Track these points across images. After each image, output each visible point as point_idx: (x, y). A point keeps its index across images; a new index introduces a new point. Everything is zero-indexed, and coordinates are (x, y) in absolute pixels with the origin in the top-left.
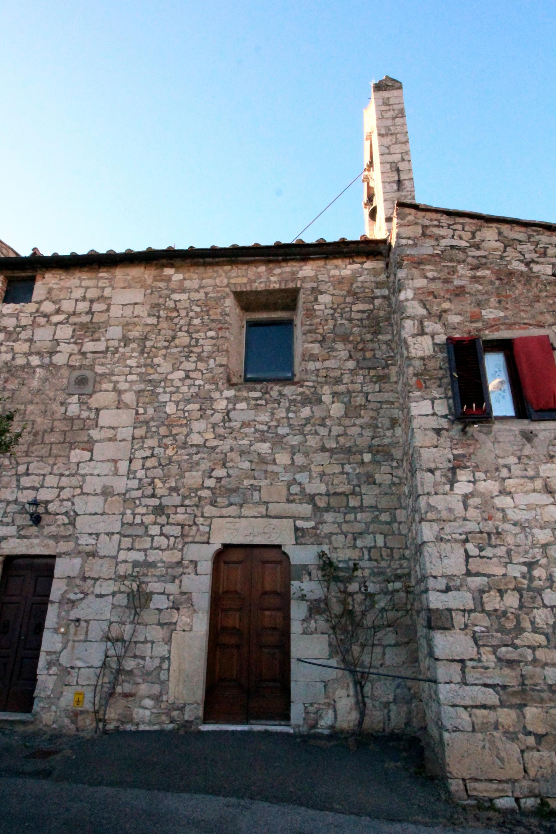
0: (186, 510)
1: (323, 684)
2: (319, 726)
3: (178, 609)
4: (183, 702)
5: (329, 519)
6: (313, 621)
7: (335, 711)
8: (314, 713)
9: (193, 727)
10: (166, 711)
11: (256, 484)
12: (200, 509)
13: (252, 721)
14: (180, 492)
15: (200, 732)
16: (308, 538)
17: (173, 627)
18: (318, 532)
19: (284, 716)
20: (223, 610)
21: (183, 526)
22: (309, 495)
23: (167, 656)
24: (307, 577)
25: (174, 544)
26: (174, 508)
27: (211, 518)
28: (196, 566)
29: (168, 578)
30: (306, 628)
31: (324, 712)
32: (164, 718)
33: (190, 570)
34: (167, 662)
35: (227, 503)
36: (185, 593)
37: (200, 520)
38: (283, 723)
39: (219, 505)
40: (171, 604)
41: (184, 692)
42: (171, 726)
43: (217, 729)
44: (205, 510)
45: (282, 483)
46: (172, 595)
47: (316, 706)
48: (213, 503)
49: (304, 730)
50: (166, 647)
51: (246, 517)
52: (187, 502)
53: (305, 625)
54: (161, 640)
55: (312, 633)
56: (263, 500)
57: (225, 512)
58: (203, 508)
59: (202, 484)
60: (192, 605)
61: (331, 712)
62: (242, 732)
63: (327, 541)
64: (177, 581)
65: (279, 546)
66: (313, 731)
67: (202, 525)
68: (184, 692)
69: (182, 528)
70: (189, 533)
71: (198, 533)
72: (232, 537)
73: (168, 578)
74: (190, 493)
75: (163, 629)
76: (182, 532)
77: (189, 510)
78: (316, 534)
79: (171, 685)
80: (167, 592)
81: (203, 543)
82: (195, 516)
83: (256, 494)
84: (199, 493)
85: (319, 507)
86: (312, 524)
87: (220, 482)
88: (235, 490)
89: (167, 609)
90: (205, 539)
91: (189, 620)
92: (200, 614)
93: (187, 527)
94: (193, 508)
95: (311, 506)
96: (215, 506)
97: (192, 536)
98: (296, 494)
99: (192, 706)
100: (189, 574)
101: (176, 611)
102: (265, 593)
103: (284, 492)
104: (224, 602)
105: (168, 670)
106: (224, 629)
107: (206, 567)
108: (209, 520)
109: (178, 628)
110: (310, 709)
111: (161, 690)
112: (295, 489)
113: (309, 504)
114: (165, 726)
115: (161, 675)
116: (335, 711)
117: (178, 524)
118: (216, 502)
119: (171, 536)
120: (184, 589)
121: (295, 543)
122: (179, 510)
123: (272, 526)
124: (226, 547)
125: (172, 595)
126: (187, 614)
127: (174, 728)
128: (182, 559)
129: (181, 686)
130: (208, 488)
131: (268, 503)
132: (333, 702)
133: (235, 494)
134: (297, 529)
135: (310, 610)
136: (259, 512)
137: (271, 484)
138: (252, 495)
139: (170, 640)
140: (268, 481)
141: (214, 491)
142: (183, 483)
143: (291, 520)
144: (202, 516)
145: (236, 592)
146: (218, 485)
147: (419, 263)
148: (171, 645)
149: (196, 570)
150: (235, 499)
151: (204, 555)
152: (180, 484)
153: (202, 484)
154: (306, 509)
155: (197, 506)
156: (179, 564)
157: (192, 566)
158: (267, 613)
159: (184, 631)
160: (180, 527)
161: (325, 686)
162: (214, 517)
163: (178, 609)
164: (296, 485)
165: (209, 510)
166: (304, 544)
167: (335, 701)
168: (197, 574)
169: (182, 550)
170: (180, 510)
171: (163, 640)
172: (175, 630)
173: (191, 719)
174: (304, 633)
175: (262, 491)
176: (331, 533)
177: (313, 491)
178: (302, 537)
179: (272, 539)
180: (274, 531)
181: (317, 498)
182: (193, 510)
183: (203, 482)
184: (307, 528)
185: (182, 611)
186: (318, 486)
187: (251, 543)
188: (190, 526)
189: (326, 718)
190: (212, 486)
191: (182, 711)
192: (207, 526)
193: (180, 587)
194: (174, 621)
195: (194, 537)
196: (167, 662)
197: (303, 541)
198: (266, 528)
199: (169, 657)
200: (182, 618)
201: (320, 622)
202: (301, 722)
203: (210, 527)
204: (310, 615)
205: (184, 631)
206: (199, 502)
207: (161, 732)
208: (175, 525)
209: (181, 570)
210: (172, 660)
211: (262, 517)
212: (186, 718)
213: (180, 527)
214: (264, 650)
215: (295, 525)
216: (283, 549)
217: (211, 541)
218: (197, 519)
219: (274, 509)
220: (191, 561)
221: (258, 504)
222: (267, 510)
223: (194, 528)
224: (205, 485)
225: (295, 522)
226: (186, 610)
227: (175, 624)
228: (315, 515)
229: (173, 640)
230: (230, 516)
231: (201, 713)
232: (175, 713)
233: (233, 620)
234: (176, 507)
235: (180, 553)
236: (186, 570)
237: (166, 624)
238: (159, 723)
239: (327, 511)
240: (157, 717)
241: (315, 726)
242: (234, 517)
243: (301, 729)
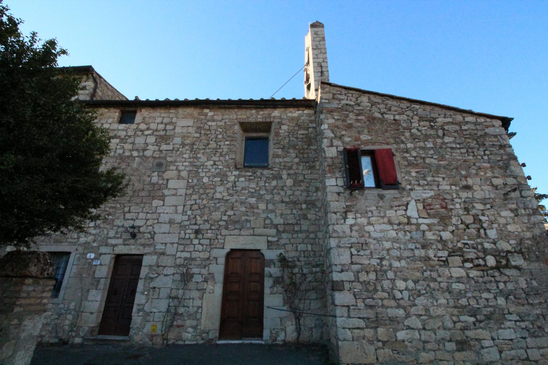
3: (207, 282)
7: (286, 333)
15: (217, 345)
19: (261, 336)
21: (210, 240)
27: (225, 235)
28: (217, 260)
32: (198, 337)
33: (214, 262)
35: (233, 228)
36: (211, 274)
42: (202, 342)
44: (222, 232)
48: (226, 228)
49: (270, 342)
50: (200, 301)
52: (213, 228)
53: (271, 290)
55: (275, 294)
57: (232, 233)
61: (283, 333)
64: (207, 268)
65: (259, 250)
79: (203, 321)
84: (219, 223)
86: (276, 239)
88: (237, 222)
90: (222, 246)
91: (212, 287)
103: (262, 223)
105: (201, 313)
107: (222, 260)
109: (207, 291)
110: (273, 332)
112: (268, 221)
116: (286, 333)
117: (208, 239)
120: (210, 272)
122: (209, 231)
124: (232, 250)
128: (210, 256)
130: (224, 220)
134: (268, 242)
135: (274, 282)
139: (202, 298)
140: (254, 218)
143: (266, 237)
144: (221, 235)
150: (237, 226)
152: (209, 218)
154: (273, 231)
155: (218, 230)
156: (208, 259)
157: (215, 260)
158: (253, 284)
161: (281, 320)
162: (227, 235)
163: (207, 282)
165: (224, 232)
168: (217, 264)
169: (209, 252)
174: (271, 294)
181: (279, 226)
185: (209, 283)
188: (214, 239)
195: (216, 245)
196: (200, 309)
197: (272, 247)
200: (209, 287)
201: (279, 288)
202: (268, 338)
209: (209, 262)
211: (251, 235)
212: (210, 337)
219: (257, 231)
223: (216, 241)
227: (205, 289)
230: (235, 235)
231: (217, 335)
232: (204, 335)
233: (235, 287)
234: (207, 230)
236: (211, 262)
237: (200, 289)
239: (283, 233)
241: (275, 340)
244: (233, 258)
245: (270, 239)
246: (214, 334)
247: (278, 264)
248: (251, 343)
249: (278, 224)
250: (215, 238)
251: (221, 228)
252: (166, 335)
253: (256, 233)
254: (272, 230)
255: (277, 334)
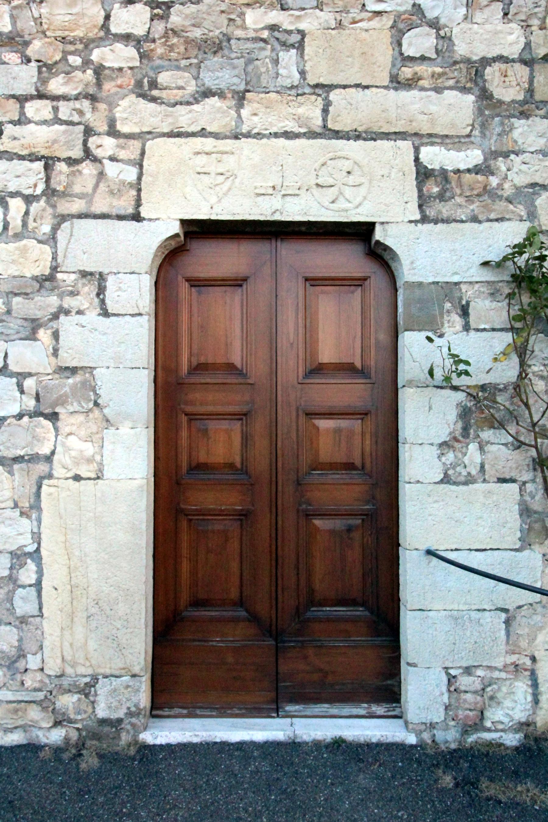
0: (56, 109)
1: (503, 616)
2: (488, 724)
3: (53, 417)
4: (90, 671)
5: (531, 138)
6: (473, 447)
7: (535, 685)
8: (475, 692)
9: (125, 738)
10: (40, 696)
11: (287, 26)
12: (102, 106)
13: (290, 708)
14: (30, 51)
15: (148, 751)
16: (458, 200)
17: (42, 468)
18: (494, 181)
19: (384, 690)
20: (192, 417)
21: (49, 163)
22: (468, 61)
23: (31, 548)
24: (457, 320)
25: (25, 224)
26: (13, 105)
27: (143, 137)
28: (101, 291)
29: (14, 324)
30: (454, 466)
31: (504, 689)
32: (34, 714)
33: (86, 299)
34: (31, 566)
35: (192, 87)
36: (74, 370)
37: (105, 146)
38: (380, 710)
39: (164, 94)
40: (31, 403)
41: (92, 645)
42: (56, 736)
43: (195, 740)
44: (119, 113)
45: (375, 23)
46: (30, 375)
47: (480, 672)
48: (147, 89)
49: (449, 737)
50: (26, 525)
51: (259, 136)
52: (56, 85)
53: (450, 457)
54: (11, 504)
55: (469, 481)
56: (312, 79)
57: (184, 118)
58: (112, 105)
59: (105, 27)
60: (96, 404)
61: (522, 688)
62: (269, 748)
63: (522, 211)
64: (44, 335)
65: (370, 227)
66: (471, 739)
67: (113, 159)
68: (92, 645)
69: (47, 167)
70: (69, 185)
71: (102, 186)
72: (213, 200)
73: (14, 324)
74: (65, 53)
75: (11, 473)
76: (48, 180)
77: (65, 110)
78: (486, 190)
79: (51, 627)
80: (13, 367)
81: (120, 218)
82: (88, 132)
83: (288, 57)
84: (96, 55)
85: (501, 102)
86: (473, 157)
87: (164, 17)
88: (217, 46)
89: (20, 416)
90: (126, 205)
91: (89, 449)
92: (125, 430)
93: (62, 167)
94: (78, 105)
95: (471, 98)
96: (154, 100)
97: (81, 196)
98: (423, 58)
99: (116, 682)
100: (80, 312)
101: (47, 424)
102: (317, 370)
103: (384, 56)
104: (197, 396)
105: (38, 585)
106: (199, 468)
107: (135, 292)
108: (136, 145)
109: (58, 471)
110: (464, 682)
111: (20, 640)
112: (419, 42)
113: (464, 90)
114: (40, 734)
115: (18, 602)
116: (535, 685)
117: (33, 158)
118: (154, 84)
119: (13, 195)
120: (68, 358)
121: (418, 217)
122: (32, 109)
123: (347, 165)
124: (198, 231)
125: (30, 375)
126: (83, 433)
127: (67, 739)
128: (55, 269)
129: (79, 631)
130: (127, 38)
131: (330, 87)
132: (528, 662)
133: (217, 59)
134: (423, 174)
135: (465, 414)
136: (298, 119)
137: (340, 25)
138: (276, 62)
139: (36, 506)
140: (327, 17)
141: (147, 46)
142: (38, 21)
143: (406, 146)
144: (113, 132)
145: (230, 367)
146: (159, 27)
147: (165, 284)
148: (39, 521)
149: (103, 302)
150: (220, 73)
151: (129, 255)
152: (27, 25)
153: (105, 27)
154: (456, 108)
155: (93, 99)
156: (47, 281)
157: (88, 290)
158: (323, 424)
159: (77, 478)
160: (39, 165)
161: (507, 622)
162: (151, 134)
163: (53, 417)
164: (426, 29)
165: (134, 114)
166: (446, 221)
167: (534, 659)
168: (105, 313)
169: (51, 239)
170: (37, 109)
171: (16, 506)
172: (50, 476)
173: (114, 716)
174: (446, 480)
175: (308, 50)
176: (533, 185)
177: (478, 51)
178: (441, 197)
179: (342, 204)
180: (351, 180)
181: (492, 73)
182: (81, 113)
183: (107, 17)
184: (458, 171)
185: (67, 422)
186: (496, 33)
187: (277, 217)
188: (71, 162)
189: (508, 703)
190: (140, 31)
191: (87, 695)
192: (129, 162)
193: (56, 352)
194: (45, 450)
195: (88, 197)
196: (31, 566)
197: (445, 209)
198: (323, 172)
199: (38, 550)
200: (71, 441)
201: (497, 449)
202: (438, 716)
203: (141, 166)
204: (466, 430)
205: (77, 478)
206: (99, 84)
207: (32, 748)
208: (22, 158)
209: (53, 301)
210: (45, 560)
211: (312, 135)
212: (102, 712)
213: (39, 165)
214: (317, 522)
215: (417, 160)
216: (378, 235)
217: (144, 213)
218: (93, 142)
219: (349, 110)
220: (84, 274)
221: (295, 91)
222: (325, 111)
223: (88, 169)
224: (114, 29)
225: (417, 150)
226: (81, 418)
227: (49, 459)
228: (484, 126)
229: (44, 504)
230: (203, 133)
231: (144, 698)
232: (68, 702)
233: (223, 444)
234: (22, 100)
235: (47, 249)
236: (68, 302)
237: (17, 459)
238: (24, 728)
239: (524, 115)
240: (16, 711)
241: (478, 725)
242: (216, 136)
243: (440, 735)
244: (196, 283)
245: (434, 156)
246: (123, 692)
247: (489, 310)
248: (338, 744)
249: (486, 62)
250: (77, 153)
251: (108, 86)
252: (112, 187)
253: (341, 121)
254: (451, 96)
255: (487, 694)
